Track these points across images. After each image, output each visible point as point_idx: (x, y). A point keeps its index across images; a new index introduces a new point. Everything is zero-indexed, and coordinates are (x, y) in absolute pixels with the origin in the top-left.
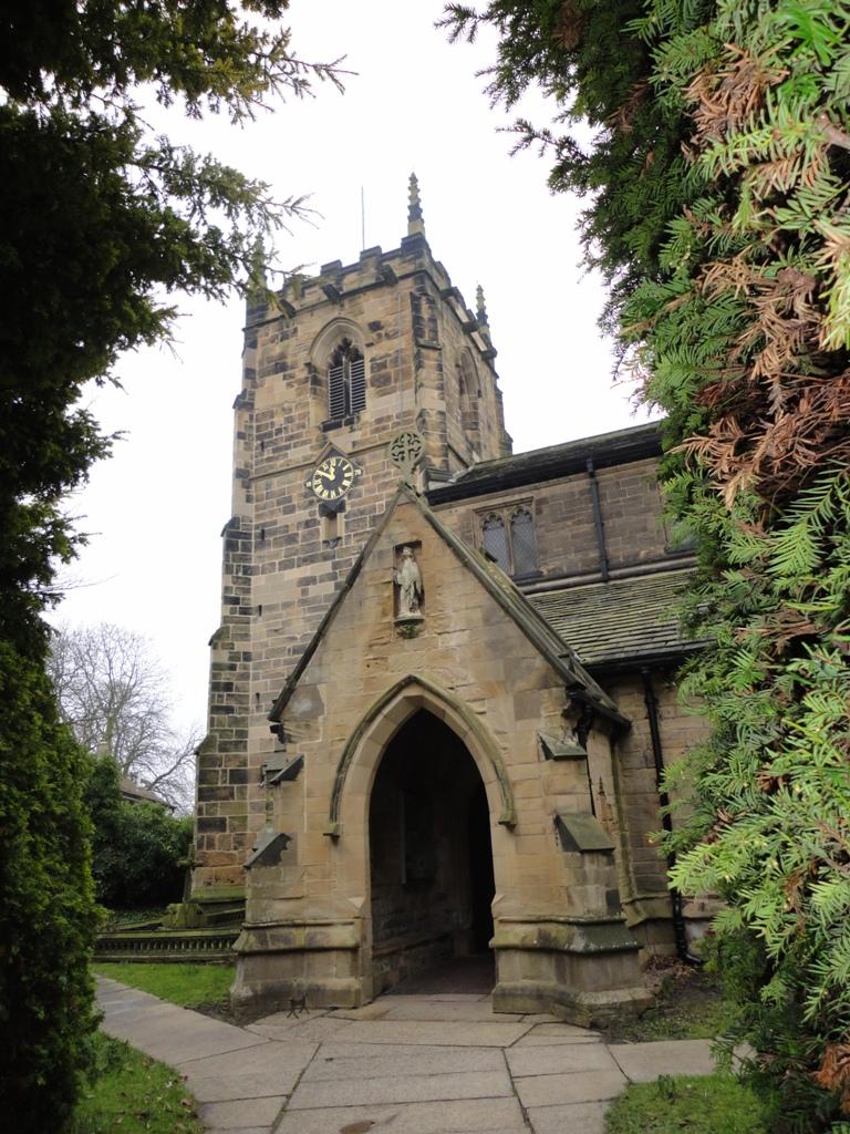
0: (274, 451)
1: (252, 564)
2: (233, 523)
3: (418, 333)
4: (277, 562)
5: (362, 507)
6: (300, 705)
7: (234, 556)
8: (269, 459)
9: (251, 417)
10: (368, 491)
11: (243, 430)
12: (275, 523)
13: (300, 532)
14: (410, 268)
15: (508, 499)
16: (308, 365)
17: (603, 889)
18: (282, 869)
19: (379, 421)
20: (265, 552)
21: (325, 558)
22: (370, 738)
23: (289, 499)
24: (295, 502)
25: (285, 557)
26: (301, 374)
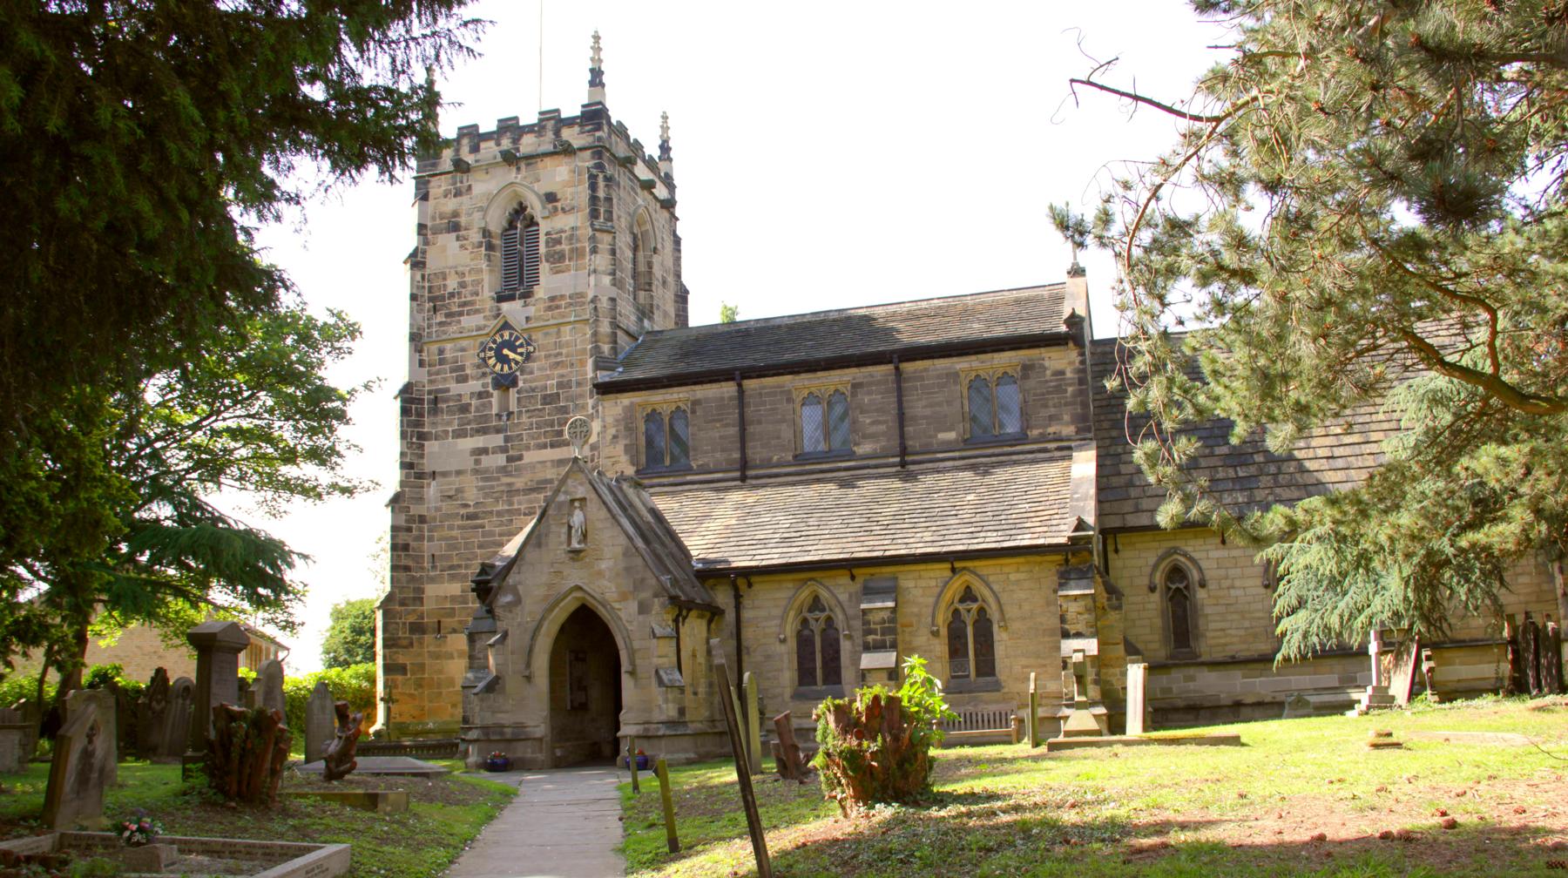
5: (533, 385)
9: (423, 277)
10: (540, 369)
12: (447, 390)
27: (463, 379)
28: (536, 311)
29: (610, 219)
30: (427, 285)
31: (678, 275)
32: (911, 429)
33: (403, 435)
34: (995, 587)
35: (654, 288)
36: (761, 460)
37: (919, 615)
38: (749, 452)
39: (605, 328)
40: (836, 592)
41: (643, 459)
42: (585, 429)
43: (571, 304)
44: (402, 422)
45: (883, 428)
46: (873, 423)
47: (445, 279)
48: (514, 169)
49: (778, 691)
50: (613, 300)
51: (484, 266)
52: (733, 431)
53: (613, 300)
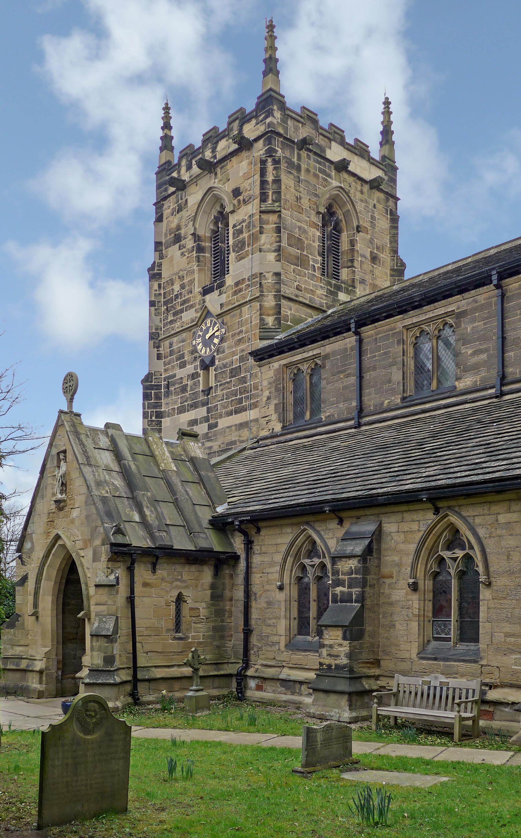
0: (175, 314)
1: (163, 410)
2: (148, 378)
3: (263, 198)
4: (176, 407)
5: (224, 362)
6: (27, 545)
7: (148, 404)
8: (171, 322)
9: (160, 286)
10: (230, 347)
11: (153, 299)
12: (174, 376)
13: (189, 383)
14: (262, 129)
15: (305, 355)
16: (194, 234)
17: (103, 655)
18: (17, 631)
19: (237, 284)
20: (169, 400)
21: (203, 405)
22: (48, 566)
23: (182, 356)
24: (186, 358)
25: (181, 403)
26: (190, 243)
27: (183, 365)
28: (228, 297)
29: (278, 200)
30: (162, 292)
31: (395, 251)
32: (512, 354)
33: (145, 415)
34: (481, 532)
35: (356, 264)
36: (375, 406)
37: (399, 565)
38: (365, 399)
39: (270, 302)
40: (326, 537)
41: (290, 416)
42: (66, 385)
43: (249, 286)
44: (144, 405)
45: (484, 356)
46: (474, 353)
47: (172, 284)
48: (213, 175)
49: (275, 639)
50: (278, 274)
51: (195, 268)
52: (353, 380)
53: (278, 274)
